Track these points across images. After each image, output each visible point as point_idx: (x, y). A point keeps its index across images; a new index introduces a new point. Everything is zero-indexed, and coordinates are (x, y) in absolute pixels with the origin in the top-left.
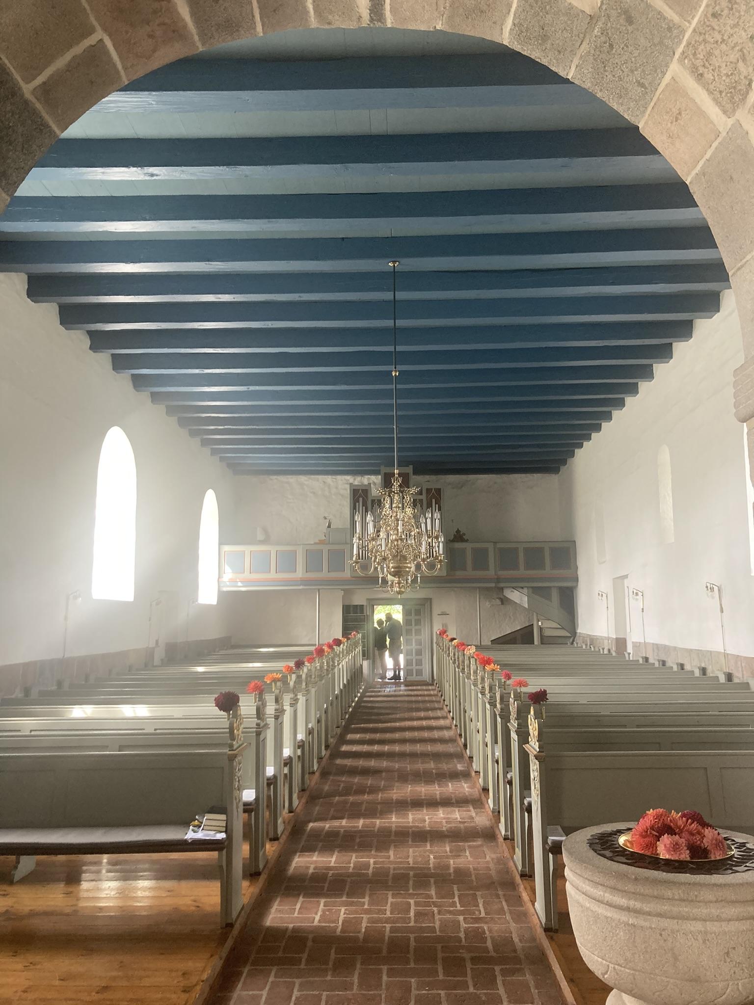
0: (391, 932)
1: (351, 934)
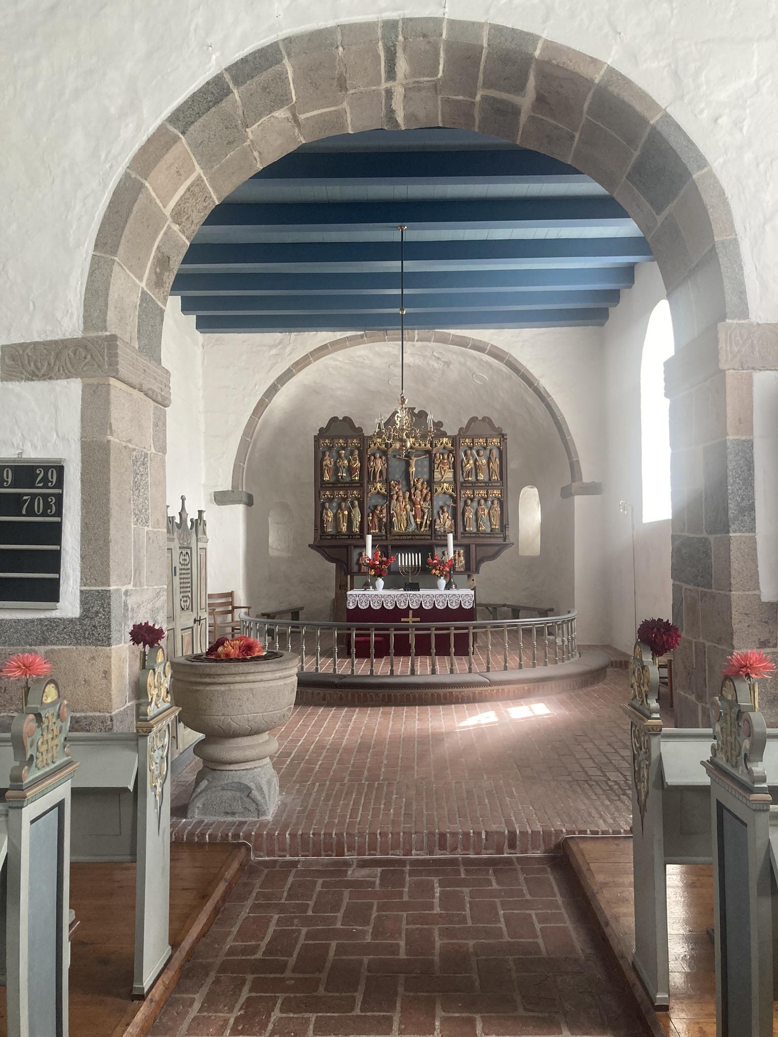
0: (389, 1020)
1: (457, 1015)
